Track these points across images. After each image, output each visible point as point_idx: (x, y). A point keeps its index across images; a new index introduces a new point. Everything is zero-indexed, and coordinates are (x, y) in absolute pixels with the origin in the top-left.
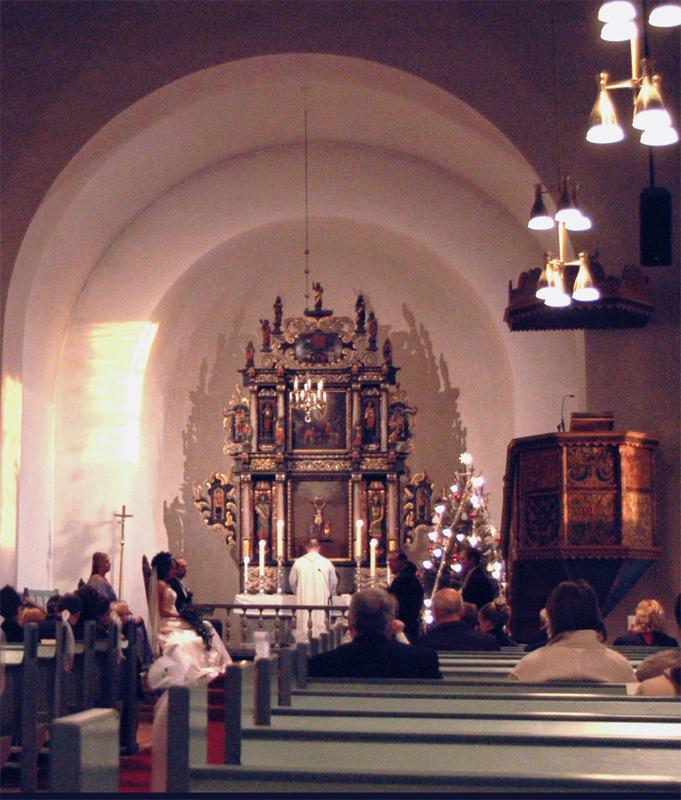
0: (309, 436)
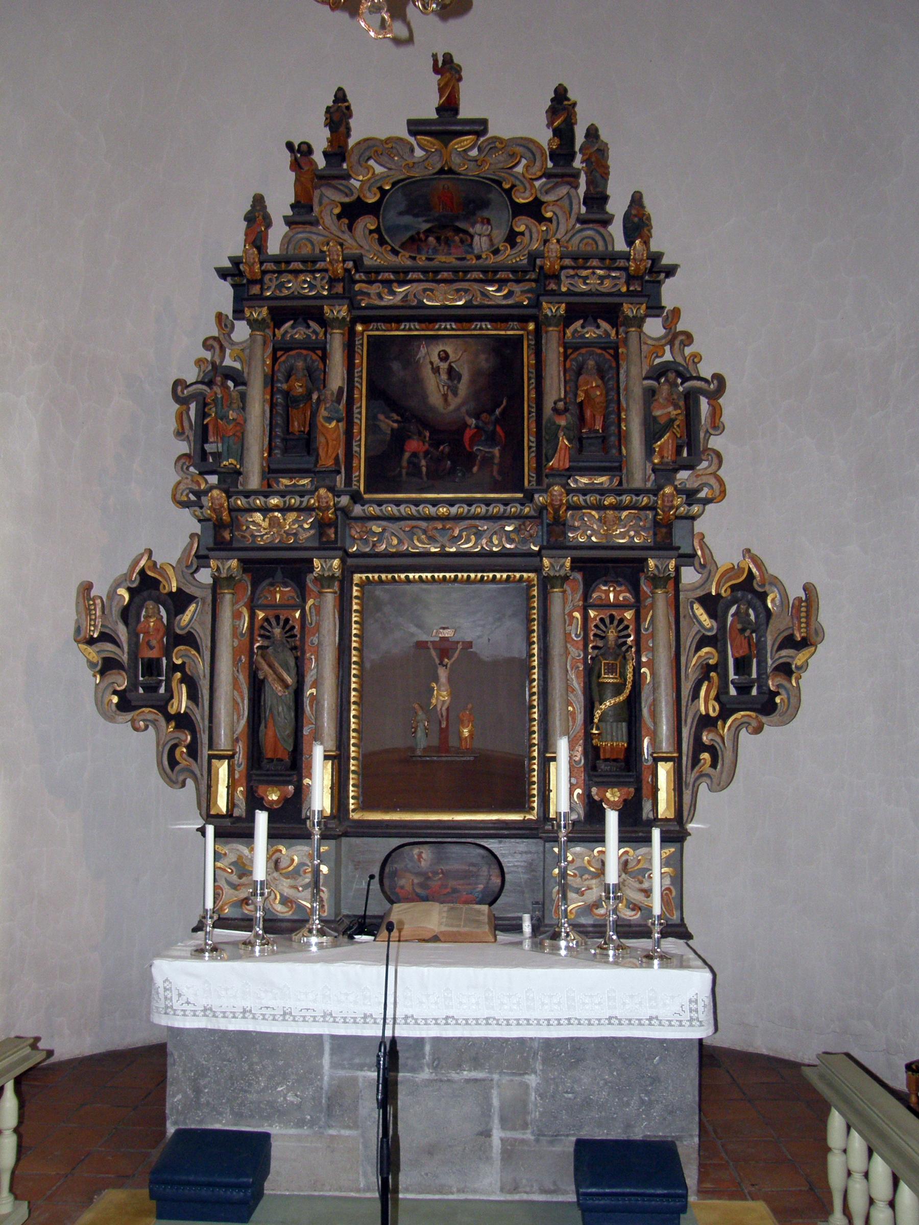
0: (414, 455)
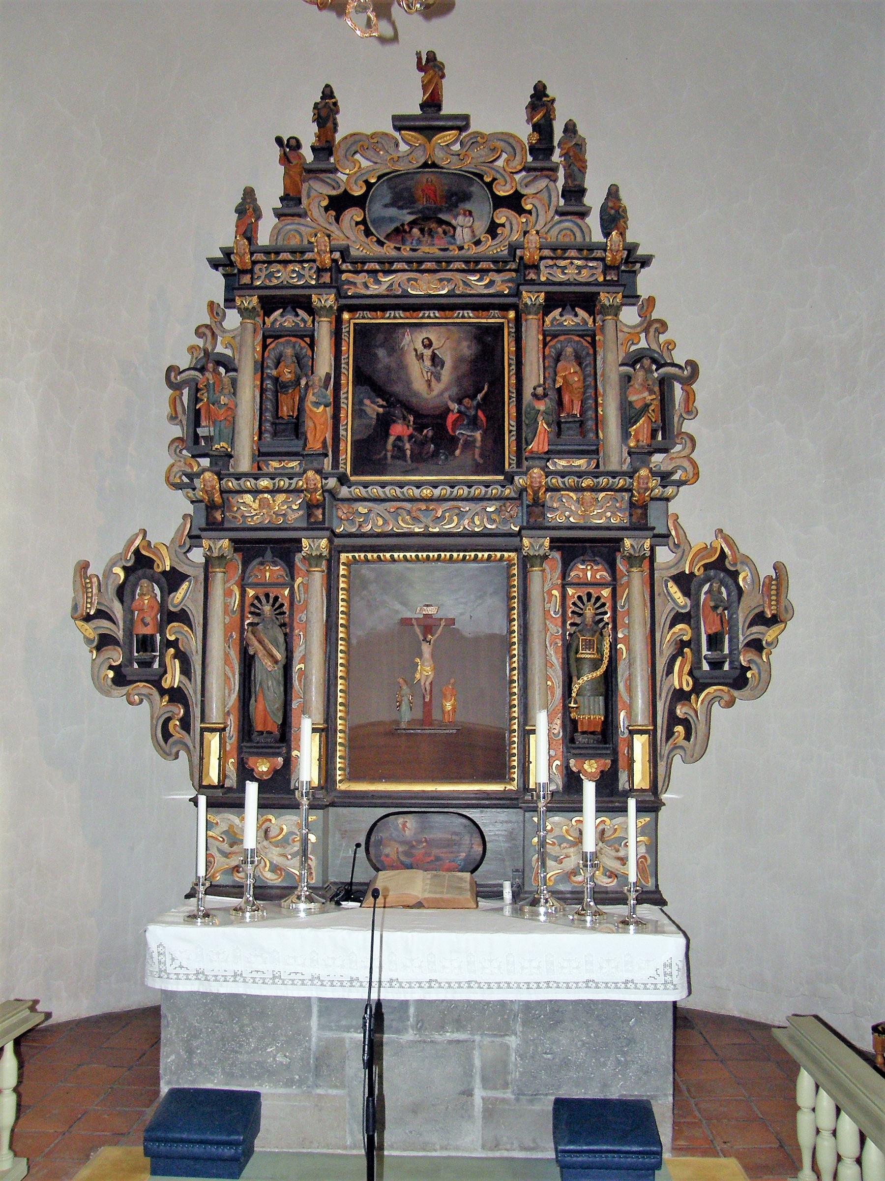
0: (399, 438)
